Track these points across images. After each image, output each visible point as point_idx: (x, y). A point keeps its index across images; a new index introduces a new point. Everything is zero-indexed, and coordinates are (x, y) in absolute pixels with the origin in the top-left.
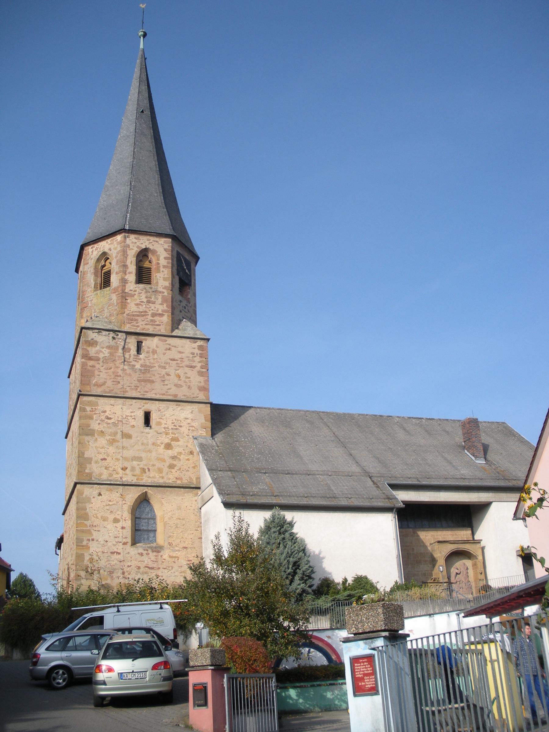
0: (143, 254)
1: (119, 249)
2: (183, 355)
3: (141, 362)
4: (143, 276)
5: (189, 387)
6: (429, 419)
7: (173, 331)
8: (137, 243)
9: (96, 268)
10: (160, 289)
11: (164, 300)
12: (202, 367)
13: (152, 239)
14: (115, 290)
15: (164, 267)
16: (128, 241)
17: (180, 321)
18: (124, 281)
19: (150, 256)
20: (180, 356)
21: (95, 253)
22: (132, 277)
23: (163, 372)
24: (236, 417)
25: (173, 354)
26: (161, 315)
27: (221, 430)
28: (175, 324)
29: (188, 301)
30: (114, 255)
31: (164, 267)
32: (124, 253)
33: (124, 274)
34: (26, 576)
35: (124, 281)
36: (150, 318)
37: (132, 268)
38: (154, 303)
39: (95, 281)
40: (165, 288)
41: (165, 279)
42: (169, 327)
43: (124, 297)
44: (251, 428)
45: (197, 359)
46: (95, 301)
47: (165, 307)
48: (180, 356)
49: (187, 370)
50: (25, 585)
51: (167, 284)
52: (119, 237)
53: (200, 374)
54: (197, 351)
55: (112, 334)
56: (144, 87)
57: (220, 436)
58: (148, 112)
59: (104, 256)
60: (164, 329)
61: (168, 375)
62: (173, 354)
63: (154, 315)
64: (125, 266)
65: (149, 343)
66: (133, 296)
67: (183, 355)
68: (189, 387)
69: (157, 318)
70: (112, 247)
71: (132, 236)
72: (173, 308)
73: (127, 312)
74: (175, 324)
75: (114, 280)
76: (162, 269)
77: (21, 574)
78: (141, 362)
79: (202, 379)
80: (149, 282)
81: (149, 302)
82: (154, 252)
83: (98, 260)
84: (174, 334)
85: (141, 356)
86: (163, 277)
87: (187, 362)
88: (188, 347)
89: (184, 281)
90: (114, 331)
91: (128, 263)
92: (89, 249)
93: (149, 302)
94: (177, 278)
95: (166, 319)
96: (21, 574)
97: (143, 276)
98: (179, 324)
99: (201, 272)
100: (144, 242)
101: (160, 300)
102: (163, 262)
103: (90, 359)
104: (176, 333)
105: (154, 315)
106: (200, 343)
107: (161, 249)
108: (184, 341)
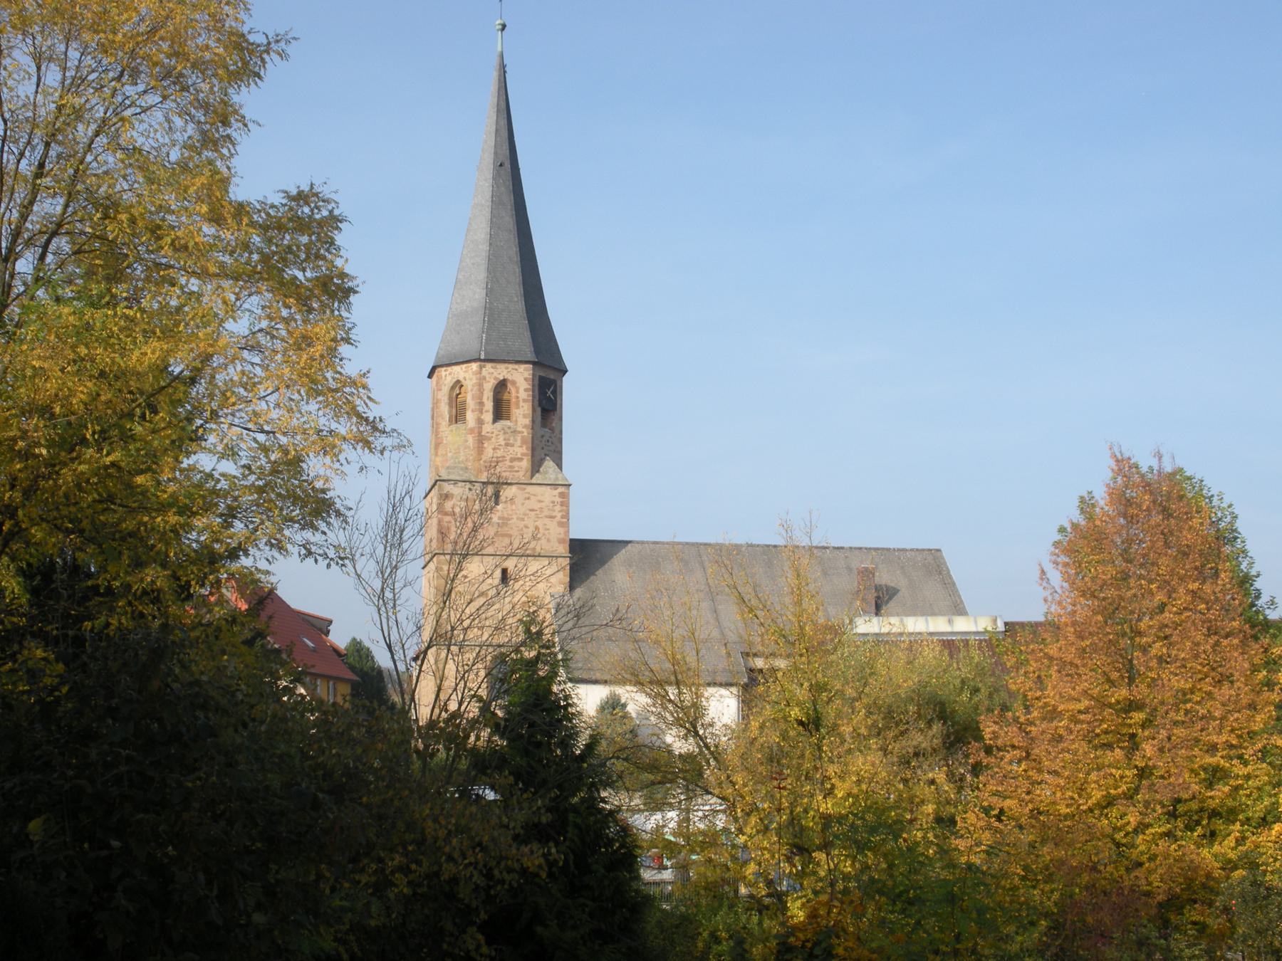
0: (501, 386)
1: (474, 381)
2: (543, 505)
3: (499, 514)
4: (500, 411)
5: (548, 540)
6: (838, 548)
7: (532, 476)
8: (494, 373)
9: (450, 398)
10: (519, 429)
11: (524, 442)
12: (562, 517)
13: (511, 366)
14: (471, 431)
15: (524, 401)
16: (484, 372)
17: (541, 462)
18: (480, 422)
19: (509, 385)
20: (539, 505)
21: (449, 378)
22: (488, 417)
23: (521, 524)
24: (603, 562)
25: (532, 504)
26: (520, 460)
27: (582, 581)
28: (536, 467)
29: (552, 430)
30: (470, 387)
31: (524, 401)
32: (480, 386)
33: (479, 410)
34: (360, 643)
35: (480, 422)
36: (508, 463)
37: (489, 405)
38: (512, 445)
39: (450, 413)
40: (525, 426)
41: (525, 416)
42: (529, 474)
43: (481, 440)
44: (617, 577)
45: (558, 508)
46: (450, 438)
47: (524, 450)
48: (539, 505)
49: (547, 521)
50: (360, 657)
51: (527, 421)
52: (474, 366)
53: (561, 524)
54: (558, 499)
55: (468, 485)
56: (504, 122)
57: (578, 592)
58: (508, 165)
59: (458, 384)
60: (521, 475)
61: (527, 527)
62: (532, 504)
63: (512, 460)
64: (481, 404)
65: (507, 493)
66: (490, 439)
67: (543, 505)
68: (548, 540)
69: (516, 463)
70: (467, 376)
71: (489, 365)
72: (533, 449)
73: (484, 458)
74: (536, 467)
75: (470, 417)
76: (521, 404)
77: (354, 639)
78: (499, 514)
79: (562, 530)
80: (508, 418)
81: (507, 445)
82: (514, 383)
83: (453, 388)
84: (534, 481)
85: (499, 507)
86: (522, 413)
87: (546, 513)
88: (549, 495)
89: (548, 402)
90: (471, 482)
91: (485, 399)
92: (442, 372)
93: (507, 445)
94: (539, 410)
95: (526, 464)
96: (354, 639)
97: (500, 411)
98: (540, 466)
99: (571, 389)
100: (502, 371)
101: (519, 443)
102: (523, 395)
103: (446, 514)
104: (538, 478)
105: (512, 460)
106: (561, 489)
107: (521, 378)
108: (544, 488)
